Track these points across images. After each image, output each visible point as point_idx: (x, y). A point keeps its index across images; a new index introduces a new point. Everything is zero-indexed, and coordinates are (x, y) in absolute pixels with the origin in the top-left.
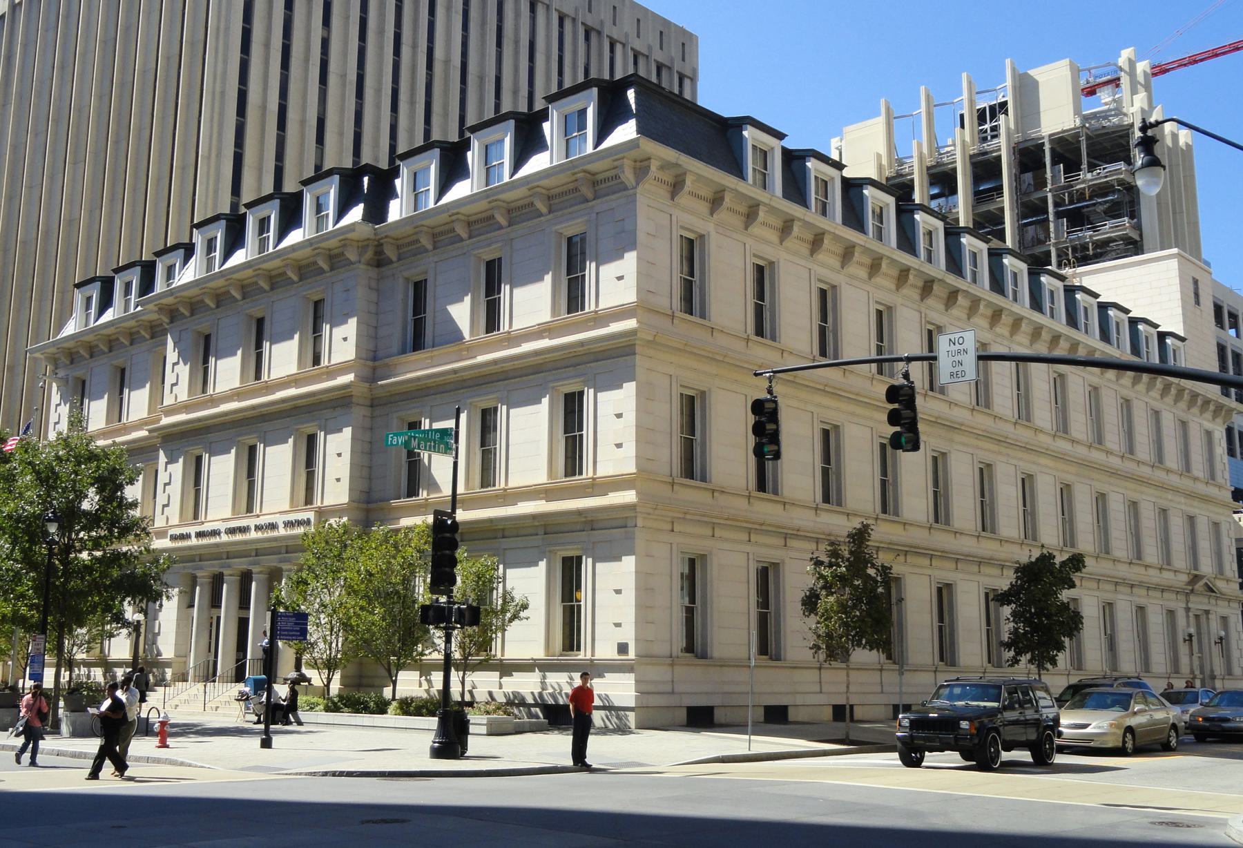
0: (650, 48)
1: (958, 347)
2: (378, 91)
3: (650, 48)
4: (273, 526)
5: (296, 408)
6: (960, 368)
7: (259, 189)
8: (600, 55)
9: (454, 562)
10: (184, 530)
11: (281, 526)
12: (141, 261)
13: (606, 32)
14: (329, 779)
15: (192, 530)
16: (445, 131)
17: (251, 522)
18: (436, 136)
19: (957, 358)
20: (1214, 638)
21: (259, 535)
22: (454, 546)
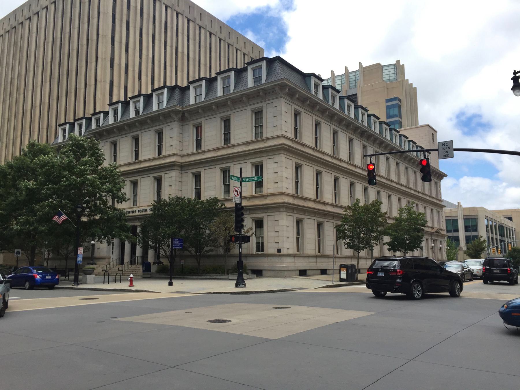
0: (249, 52)
1: (446, 146)
2: (134, 71)
3: (249, 52)
4: (145, 211)
5: (215, 160)
6: (447, 154)
7: (133, 92)
8: (233, 54)
9: (242, 220)
10: (134, 209)
11: (137, 211)
12: (236, 68)
13: (235, 46)
14: (147, 290)
15: (137, 209)
16: (171, 82)
17: (137, 209)
18: (168, 84)
19: (446, 150)
20: (438, 248)
21: (139, 214)
22: (242, 214)
